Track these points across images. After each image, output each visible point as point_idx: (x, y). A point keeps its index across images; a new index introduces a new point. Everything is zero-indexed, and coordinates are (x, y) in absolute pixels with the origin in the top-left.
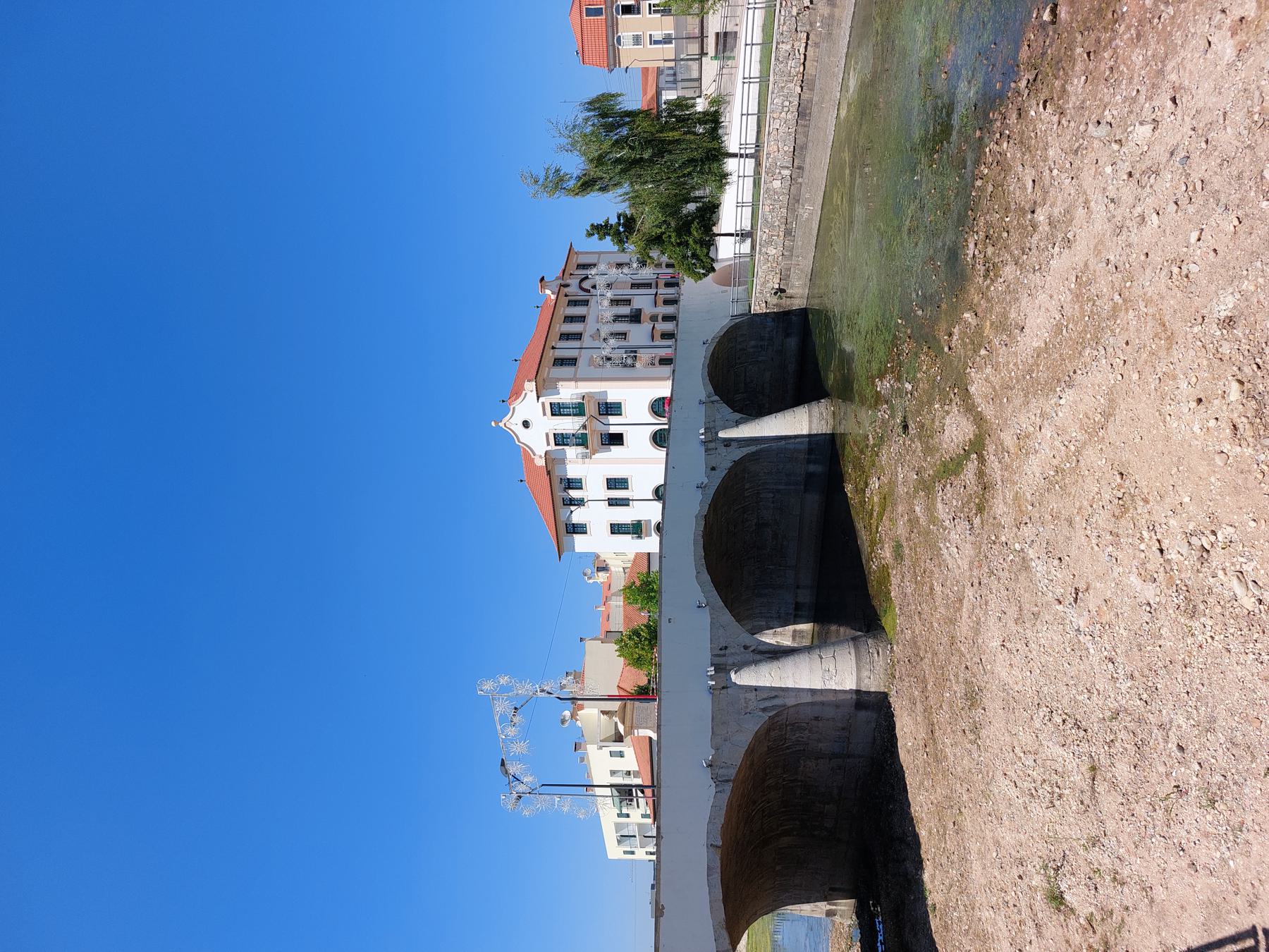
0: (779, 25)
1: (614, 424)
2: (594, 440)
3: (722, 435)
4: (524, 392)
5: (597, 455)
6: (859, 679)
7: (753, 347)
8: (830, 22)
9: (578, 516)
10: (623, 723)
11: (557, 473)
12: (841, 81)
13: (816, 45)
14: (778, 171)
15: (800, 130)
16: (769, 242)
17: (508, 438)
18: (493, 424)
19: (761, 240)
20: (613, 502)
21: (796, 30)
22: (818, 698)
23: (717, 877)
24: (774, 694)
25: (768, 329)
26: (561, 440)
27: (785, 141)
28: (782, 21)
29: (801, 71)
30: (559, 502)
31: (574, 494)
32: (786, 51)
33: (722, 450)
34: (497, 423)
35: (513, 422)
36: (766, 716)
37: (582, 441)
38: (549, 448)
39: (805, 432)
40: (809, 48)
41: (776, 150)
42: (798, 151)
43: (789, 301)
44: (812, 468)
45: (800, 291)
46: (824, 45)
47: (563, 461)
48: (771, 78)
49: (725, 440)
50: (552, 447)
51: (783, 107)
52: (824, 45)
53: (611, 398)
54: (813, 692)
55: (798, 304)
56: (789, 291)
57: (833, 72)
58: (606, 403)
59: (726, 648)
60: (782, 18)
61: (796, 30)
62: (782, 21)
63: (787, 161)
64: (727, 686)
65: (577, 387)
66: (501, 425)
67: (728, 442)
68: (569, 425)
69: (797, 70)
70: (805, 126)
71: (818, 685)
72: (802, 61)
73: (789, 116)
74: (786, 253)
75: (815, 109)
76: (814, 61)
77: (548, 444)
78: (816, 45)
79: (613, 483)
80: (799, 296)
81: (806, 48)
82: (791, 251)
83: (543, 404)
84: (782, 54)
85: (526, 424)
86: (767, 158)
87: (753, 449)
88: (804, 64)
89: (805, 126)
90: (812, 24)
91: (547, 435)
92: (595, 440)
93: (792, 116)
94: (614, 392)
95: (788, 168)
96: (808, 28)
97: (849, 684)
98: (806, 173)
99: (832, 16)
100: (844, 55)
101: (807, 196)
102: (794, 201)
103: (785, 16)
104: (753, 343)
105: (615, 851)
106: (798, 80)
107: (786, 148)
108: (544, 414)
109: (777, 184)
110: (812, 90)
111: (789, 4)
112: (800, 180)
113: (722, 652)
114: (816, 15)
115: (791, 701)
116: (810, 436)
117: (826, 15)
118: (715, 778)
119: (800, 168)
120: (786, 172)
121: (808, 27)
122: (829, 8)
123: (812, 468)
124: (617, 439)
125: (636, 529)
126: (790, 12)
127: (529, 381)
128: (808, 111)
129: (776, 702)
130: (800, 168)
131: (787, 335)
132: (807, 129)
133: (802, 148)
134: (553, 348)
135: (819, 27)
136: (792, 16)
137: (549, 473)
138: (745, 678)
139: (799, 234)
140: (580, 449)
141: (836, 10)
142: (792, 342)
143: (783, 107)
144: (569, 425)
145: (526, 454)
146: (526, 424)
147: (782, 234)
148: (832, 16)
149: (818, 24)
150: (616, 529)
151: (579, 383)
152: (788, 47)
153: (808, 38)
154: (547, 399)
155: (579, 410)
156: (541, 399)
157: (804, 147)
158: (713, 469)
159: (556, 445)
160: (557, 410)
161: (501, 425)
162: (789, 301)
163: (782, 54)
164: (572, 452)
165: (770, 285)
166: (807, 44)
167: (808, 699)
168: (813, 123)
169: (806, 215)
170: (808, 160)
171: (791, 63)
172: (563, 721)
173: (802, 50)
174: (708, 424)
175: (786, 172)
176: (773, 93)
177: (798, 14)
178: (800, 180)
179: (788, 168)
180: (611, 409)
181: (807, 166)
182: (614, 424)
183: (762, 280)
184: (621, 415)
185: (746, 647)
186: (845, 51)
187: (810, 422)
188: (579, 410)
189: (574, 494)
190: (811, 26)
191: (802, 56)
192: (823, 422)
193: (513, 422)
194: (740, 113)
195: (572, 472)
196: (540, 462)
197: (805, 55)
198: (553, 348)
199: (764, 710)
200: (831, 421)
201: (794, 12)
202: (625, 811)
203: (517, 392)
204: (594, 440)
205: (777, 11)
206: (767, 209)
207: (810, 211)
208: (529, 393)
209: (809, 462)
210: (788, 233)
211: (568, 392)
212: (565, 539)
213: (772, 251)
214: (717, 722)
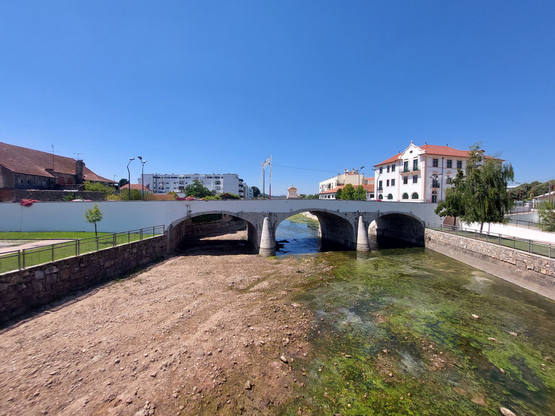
0: (521, 253)
1: (410, 181)
2: (405, 174)
3: (360, 217)
4: (421, 150)
5: (401, 176)
6: (261, 248)
7: (414, 228)
8: (518, 275)
9: (385, 170)
10: (290, 189)
11: (397, 164)
12: (493, 274)
13: (510, 268)
14: (466, 244)
15: (479, 254)
16: (444, 237)
17: (407, 146)
18: (412, 141)
19: (445, 234)
20: (388, 181)
21: (517, 260)
22: (259, 238)
23: (215, 213)
24: (261, 228)
25: (420, 233)
26: (406, 164)
27: (475, 248)
28: (522, 254)
29: (500, 259)
30: (388, 165)
31: (391, 169)
32: (509, 254)
33: (355, 217)
34: (412, 142)
35: (412, 147)
36: (255, 225)
37: (406, 170)
38: (403, 160)
39: (358, 242)
40: (509, 264)
41: (473, 244)
42: (471, 253)
43: (427, 241)
44: (349, 243)
45: (429, 246)
46: (509, 271)
47: (400, 165)
48: (500, 246)
49: (358, 218)
50: (404, 161)
51: (488, 249)
52: (509, 271)
53: (419, 180)
54: (261, 237)
55: (426, 244)
56: (430, 242)
57: (497, 272)
58: (417, 178)
59: (276, 216)
60: (523, 255)
61: (517, 260)
62: (522, 254)
63: (469, 248)
64: (264, 216)
65: (423, 168)
66: (411, 144)
67: (357, 219)
68: (411, 166)
69: (501, 257)
70: (480, 257)
71: (262, 238)
72: (504, 260)
73: (484, 251)
74: (440, 242)
75: (485, 262)
76: (504, 265)
77: (405, 160)
78: (510, 268)
79: (393, 181)
80: (429, 245)
81: (509, 263)
82: (441, 245)
83: (418, 157)
84: (508, 252)
85: (411, 152)
86: (471, 240)
87: (354, 226)
88: (503, 261)
89: (480, 257)
90: (519, 267)
91: (407, 159)
92: (405, 175)
93: (484, 252)
94: (421, 180)
95: (466, 248)
96: (518, 265)
97: (261, 246)
98: (463, 254)
99: (521, 276)
100: (503, 278)
101: (456, 253)
102: (455, 248)
103: (524, 256)
104: (416, 228)
105: (321, 184)
106: (497, 257)
107: (473, 248)
108: (414, 158)
109: (462, 243)
110: (492, 262)
111: (529, 259)
112: (462, 252)
113: (275, 215)
114: (523, 270)
115: (258, 231)
116: (356, 243)
117: (522, 274)
118: (239, 213)
119: (466, 252)
120: (465, 247)
121: (518, 265)
122: (525, 276)
123: (349, 243)
124: (406, 182)
125: (380, 188)
126: (525, 258)
127: (425, 151)
128: (485, 259)
129: (259, 228)
130: (466, 252)
131: (416, 240)
132: (478, 257)
133: (472, 254)
134: (443, 158)
135: (517, 270)
136: (523, 259)
137: (396, 161)
138: (265, 221)
139: (445, 248)
140: (403, 170)
141: (523, 279)
142: (414, 241)
143: (488, 249)
144: (411, 166)
145: (401, 152)
146: (411, 152)
147: (446, 242)
148: (521, 276)
149: (518, 270)
150: (381, 182)
151: (424, 169)
152: (511, 255)
153: (513, 264)
154: (419, 158)
155: (415, 169)
156: (419, 156)
157: (472, 255)
158: (346, 214)
159: (405, 162)
160: (415, 162)
161: (411, 144)
162: (427, 241)
163: (508, 252)
164: (402, 167)
165: (432, 236)
166: (511, 263)
167: (259, 235)
168: (480, 260)
169: (450, 252)
170: (468, 256)
171: (504, 255)
172: (345, 170)
173: (508, 261)
174: (368, 214)
175: (465, 247)
176: (494, 246)
177: (524, 262)
178: (462, 252)
179: (466, 248)
180: (415, 180)
181: (466, 255)
182: (410, 181)
183: (434, 233)
184: (413, 183)
185: (276, 221)
186: (505, 279)
187: (361, 244)
188: (415, 169)
189: (391, 169)
190: (518, 267)
191: (506, 261)
192: (360, 248)
193: (412, 147)
194: (502, 234)
195: (397, 168)
196: (399, 158)
197: (507, 262)
198: (443, 158)
199: (257, 225)
200: (360, 250)
201: (525, 261)
202: (327, 186)
203: (422, 148)
204: (405, 174)
205: (527, 253)
206: (454, 238)
207: (451, 254)
208: (421, 152)
209: (351, 242)
210: (446, 244)
211: (421, 165)
212: (379, 167)
213: (441, 238)
214: (254, 214)
